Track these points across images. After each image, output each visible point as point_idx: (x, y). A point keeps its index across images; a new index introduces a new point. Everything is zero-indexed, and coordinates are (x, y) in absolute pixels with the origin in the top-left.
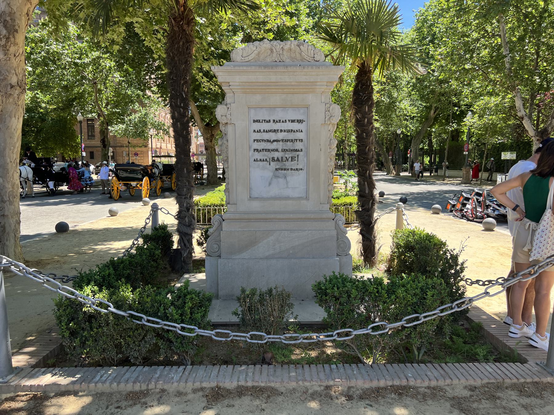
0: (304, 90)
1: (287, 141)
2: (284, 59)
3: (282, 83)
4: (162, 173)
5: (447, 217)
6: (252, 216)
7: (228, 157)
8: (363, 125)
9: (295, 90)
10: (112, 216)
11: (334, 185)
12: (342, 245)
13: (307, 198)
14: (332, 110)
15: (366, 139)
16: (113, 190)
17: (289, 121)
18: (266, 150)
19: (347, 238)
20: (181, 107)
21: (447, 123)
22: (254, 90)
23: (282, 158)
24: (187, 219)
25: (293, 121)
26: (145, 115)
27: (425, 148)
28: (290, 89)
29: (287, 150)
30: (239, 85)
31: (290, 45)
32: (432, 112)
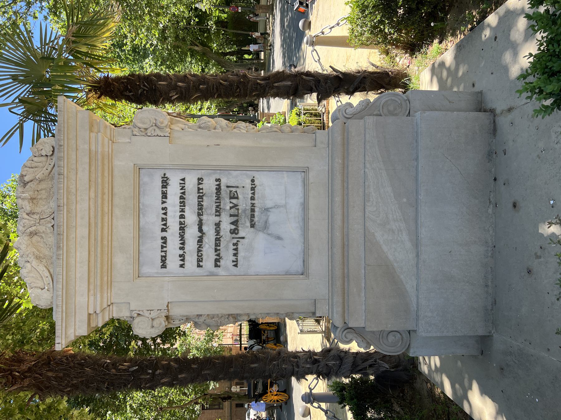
0: (106, 174)
1: (200, 207)
2: (48, 211)
3: (92, 214)
4: (259, 340)
5: (314, 11)
6: (338, 272)
7: (229, 315)
8: (188, 89)
9: (106, 191)
10: (310, 413)
12: (391, 108)
13: (305, 171)
14: (144, 123)
15: (208, 84)
16: (277, 401)
17: (163, 202)
18: (217, 245)
20: (153, 373)
21: (208, 31)
22: (105, 268)
23: (231, 216)
24: (331, 363)
25: (164, 195)
26: (198, 350)
27: (235, 59)
28: (103, 199)
29: (217, 207)
30: (95, 295)
31: (23, 199)
32: (196, 48)
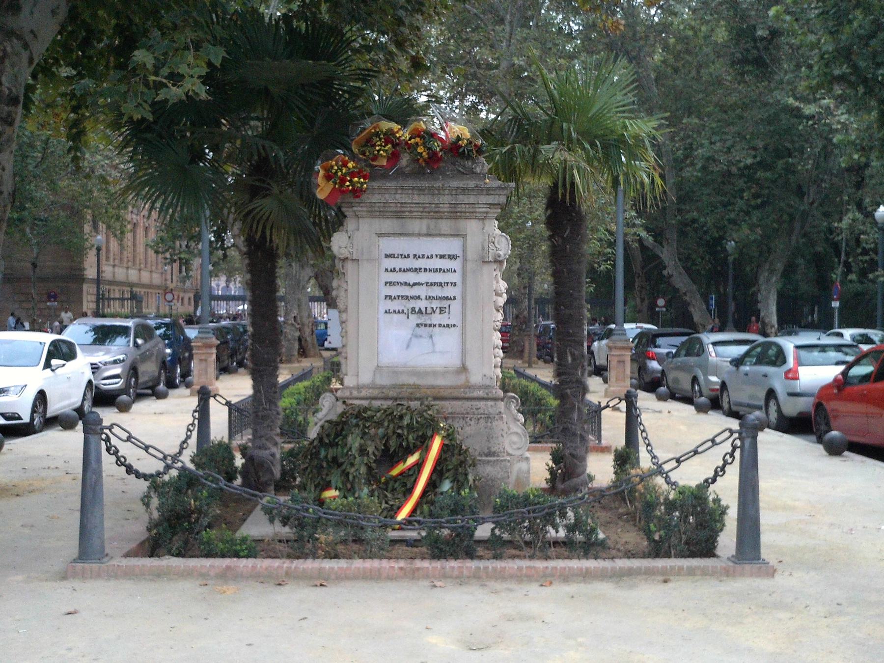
11: (667, 114)
19: (250, 272)
25: (442, 257)
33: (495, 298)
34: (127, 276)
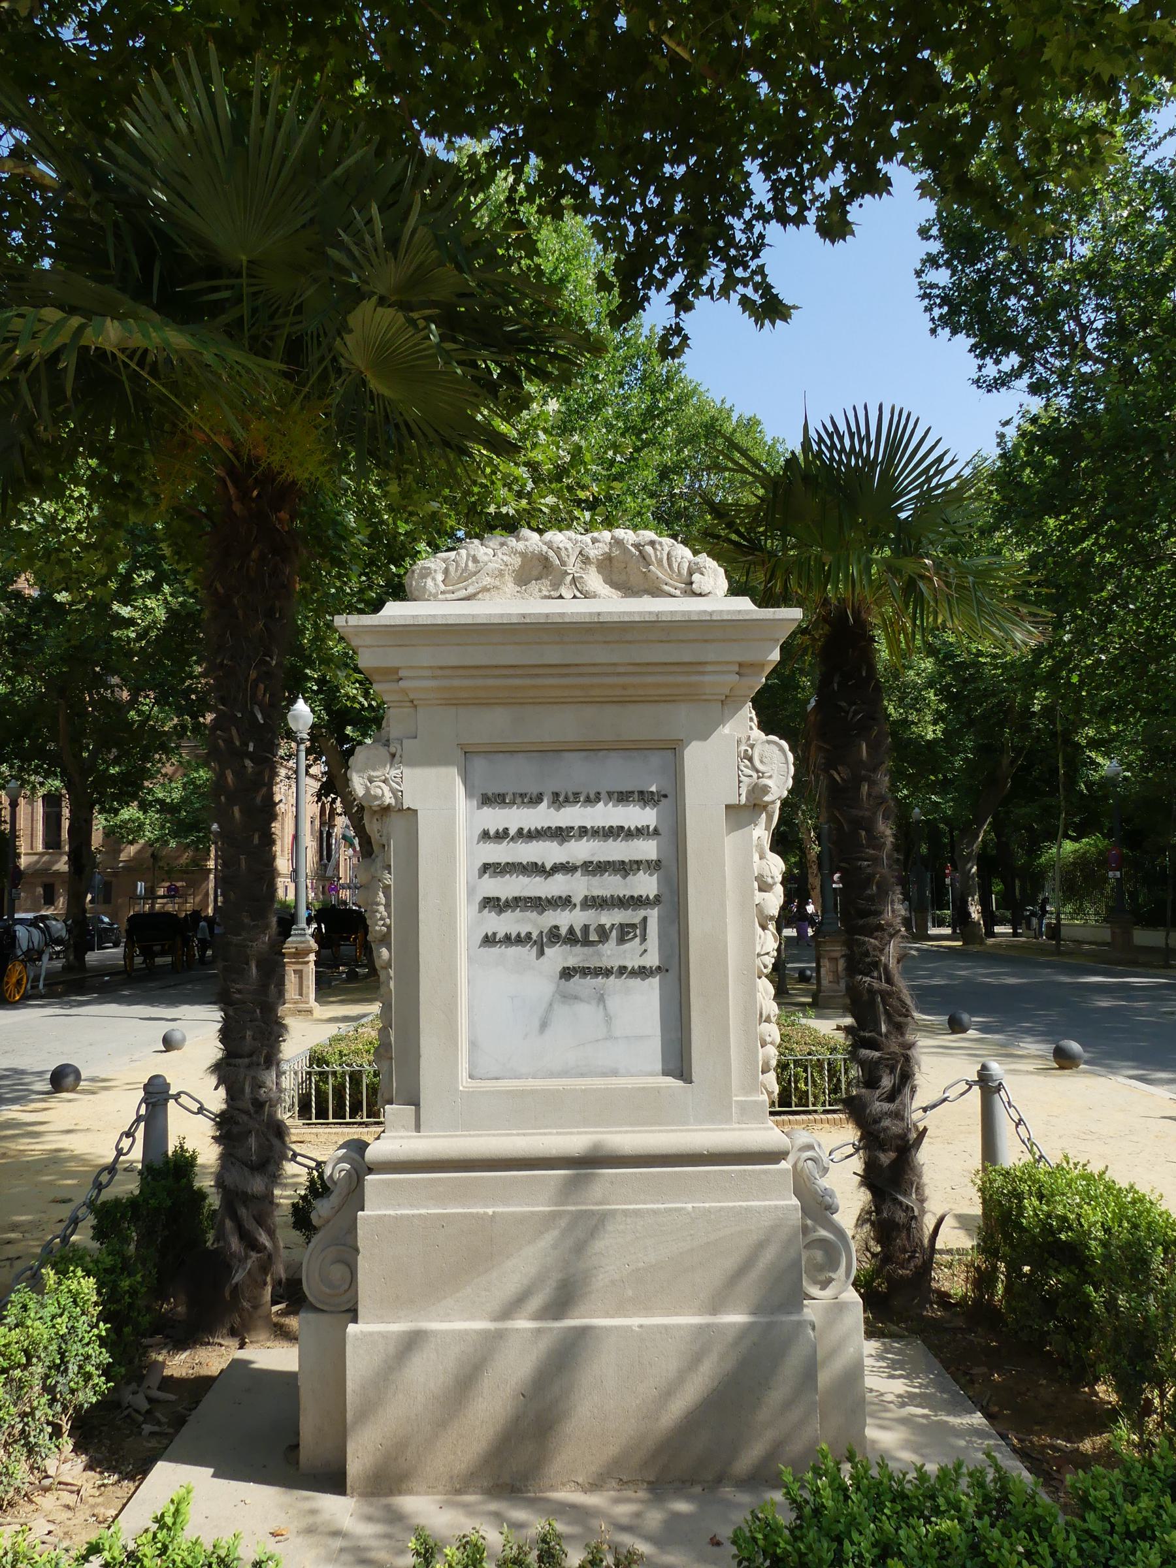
24: (252, 1141)
33: (759, 897)
34: (1168, 935)
